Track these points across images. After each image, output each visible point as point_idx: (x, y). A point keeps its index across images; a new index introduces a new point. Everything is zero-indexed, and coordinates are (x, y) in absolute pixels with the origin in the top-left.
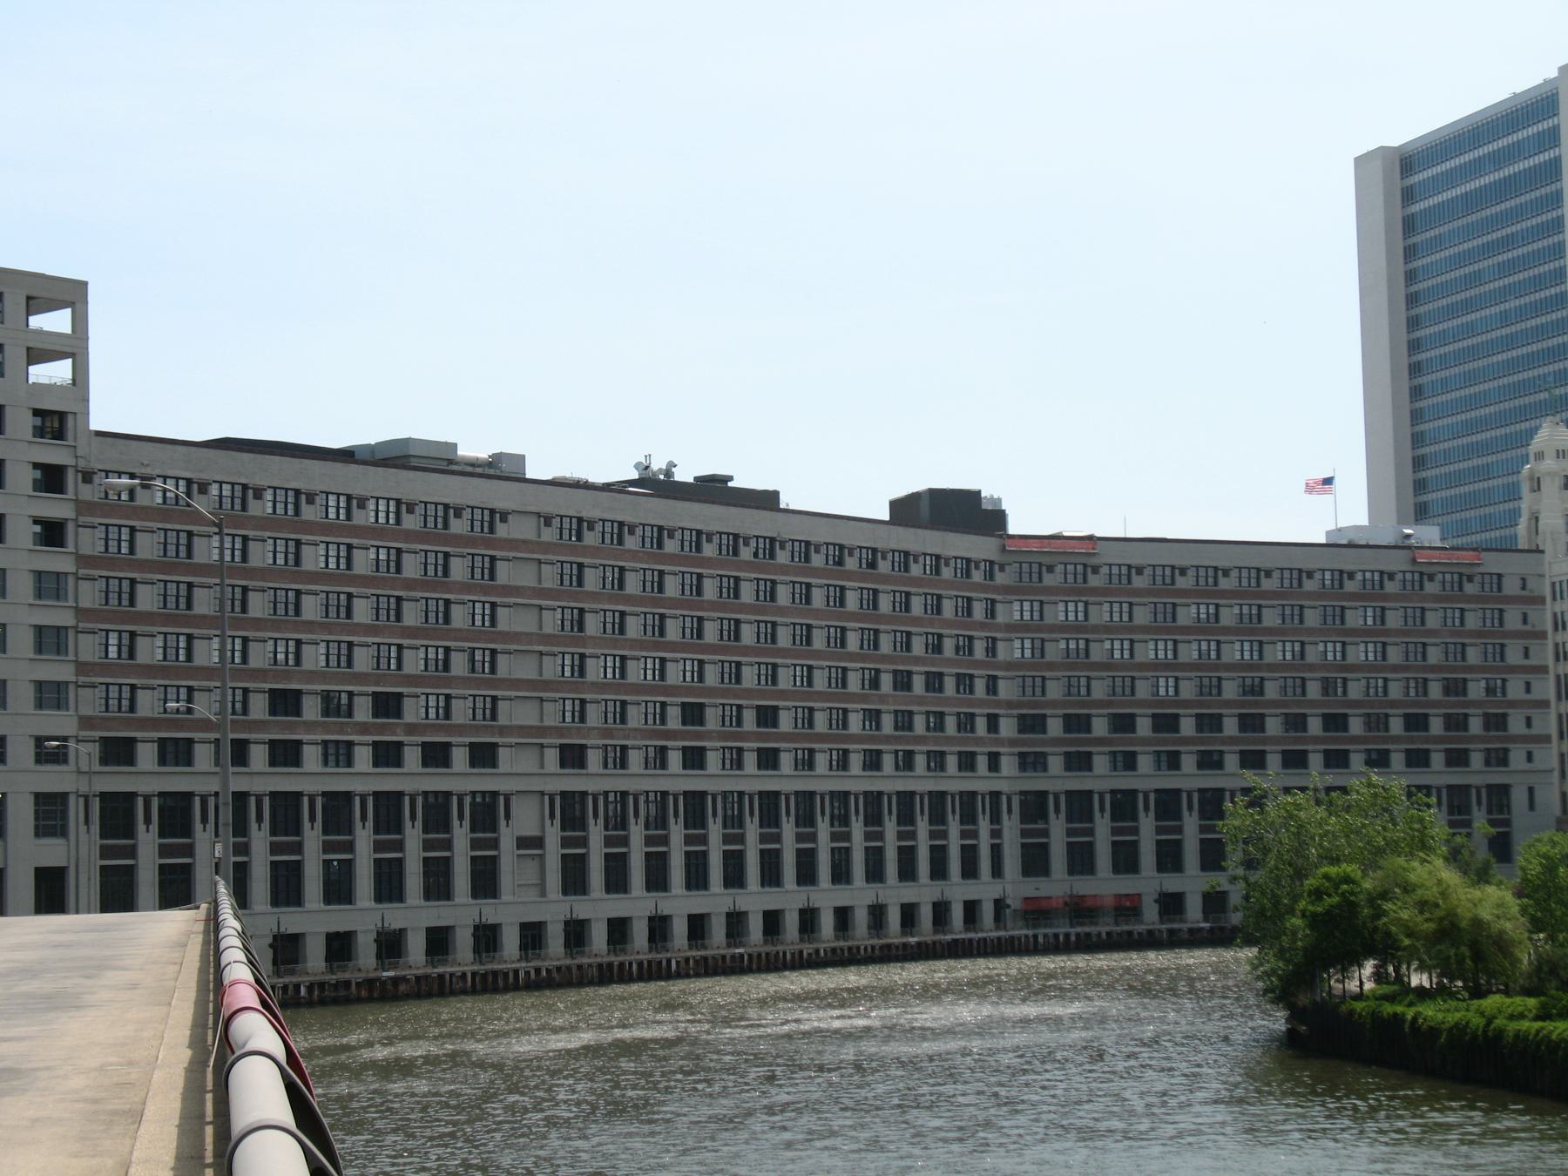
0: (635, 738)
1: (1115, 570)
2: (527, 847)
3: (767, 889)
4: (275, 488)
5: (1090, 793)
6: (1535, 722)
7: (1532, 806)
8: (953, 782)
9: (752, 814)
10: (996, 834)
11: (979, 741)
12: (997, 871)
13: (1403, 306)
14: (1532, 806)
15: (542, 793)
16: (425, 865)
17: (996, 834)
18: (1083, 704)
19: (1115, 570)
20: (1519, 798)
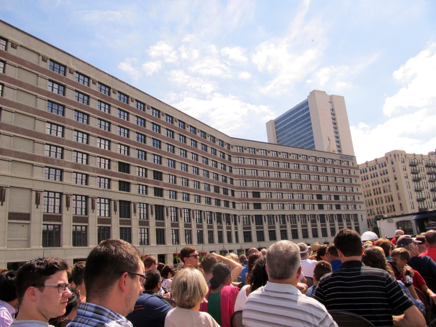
0: (94, 172)
1: (245, 217)
2: (13, 219)
3: (159, 245)
4: (140, 203)
5: (261, 216)
6: (360, 198)
7: (362, 220)
8: (223, 210)
9: (152, 214)
10: (236, 228)
11: (229, 198)
12: (237, 241)
13: (310, 113)
14: (362, 220)
15: (31, 190)
16: (78, 245)
17: (236, 228)
18: (257, 189)
19: (245, 217)
20: (359, 217)
